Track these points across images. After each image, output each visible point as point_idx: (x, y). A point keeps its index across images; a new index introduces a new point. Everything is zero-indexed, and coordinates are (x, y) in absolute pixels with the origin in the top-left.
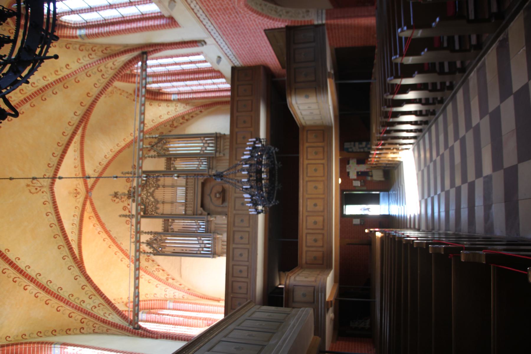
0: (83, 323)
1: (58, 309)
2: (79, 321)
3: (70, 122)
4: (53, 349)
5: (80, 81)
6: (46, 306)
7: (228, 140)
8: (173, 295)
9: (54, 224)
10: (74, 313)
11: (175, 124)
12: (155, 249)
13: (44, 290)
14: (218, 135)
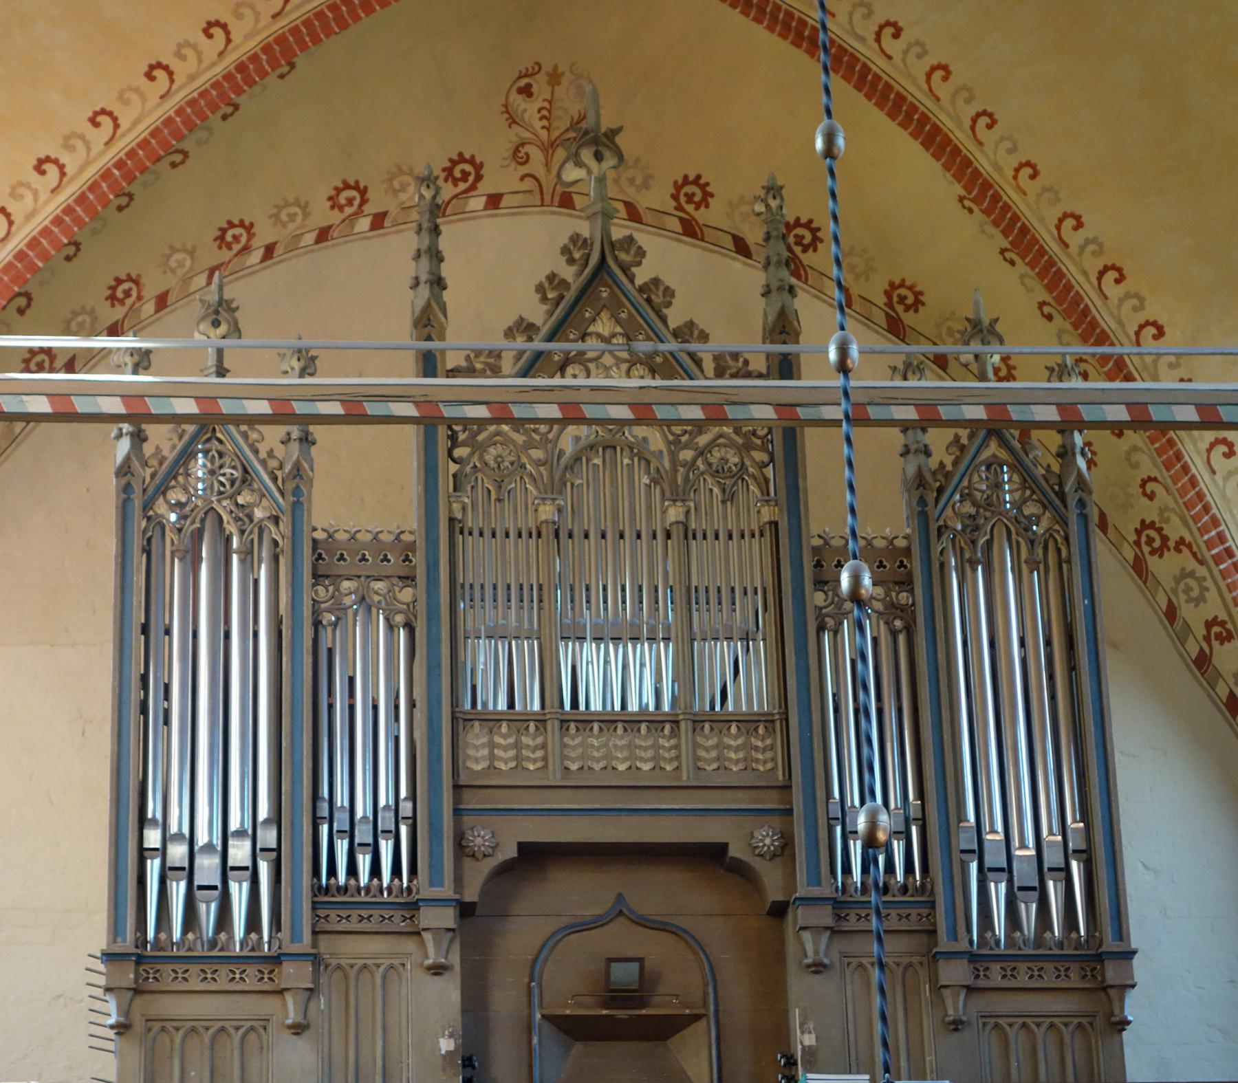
11: (1164, 567)
12: (172, 474)
14: (1112, 973)
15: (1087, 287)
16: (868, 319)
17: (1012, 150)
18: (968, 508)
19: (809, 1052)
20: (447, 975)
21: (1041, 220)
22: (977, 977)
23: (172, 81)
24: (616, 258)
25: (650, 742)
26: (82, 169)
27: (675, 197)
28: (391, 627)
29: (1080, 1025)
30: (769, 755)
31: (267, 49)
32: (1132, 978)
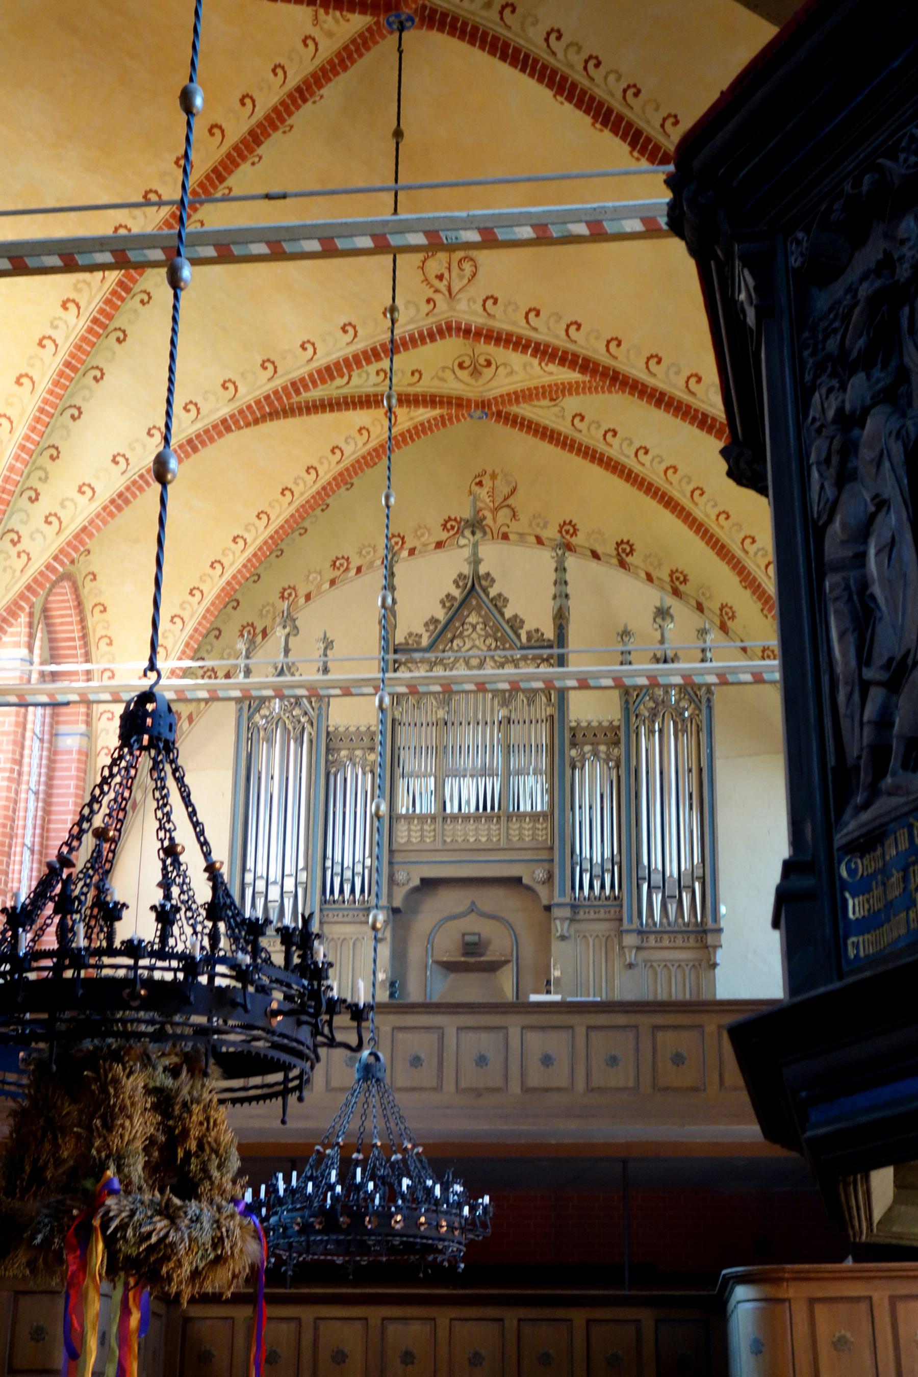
3: (699, 380)
7: (678, 991)
9: (315, 353)
14: (710, 939)
15: (760, 573)
17: (714, 506)
18: (652, 704)
19: (558, 980)
20: (384, 942)
21: (733, 540)
22: (642, 942)
23: (293, 496)
24: (481, 586)
25: (486, 827)
26: (255, 540)
27: (560, 532)
28: (364, 773)
29: (694, 966)
30: (544, 832)
31: (335, 479)
32: (720, 941)
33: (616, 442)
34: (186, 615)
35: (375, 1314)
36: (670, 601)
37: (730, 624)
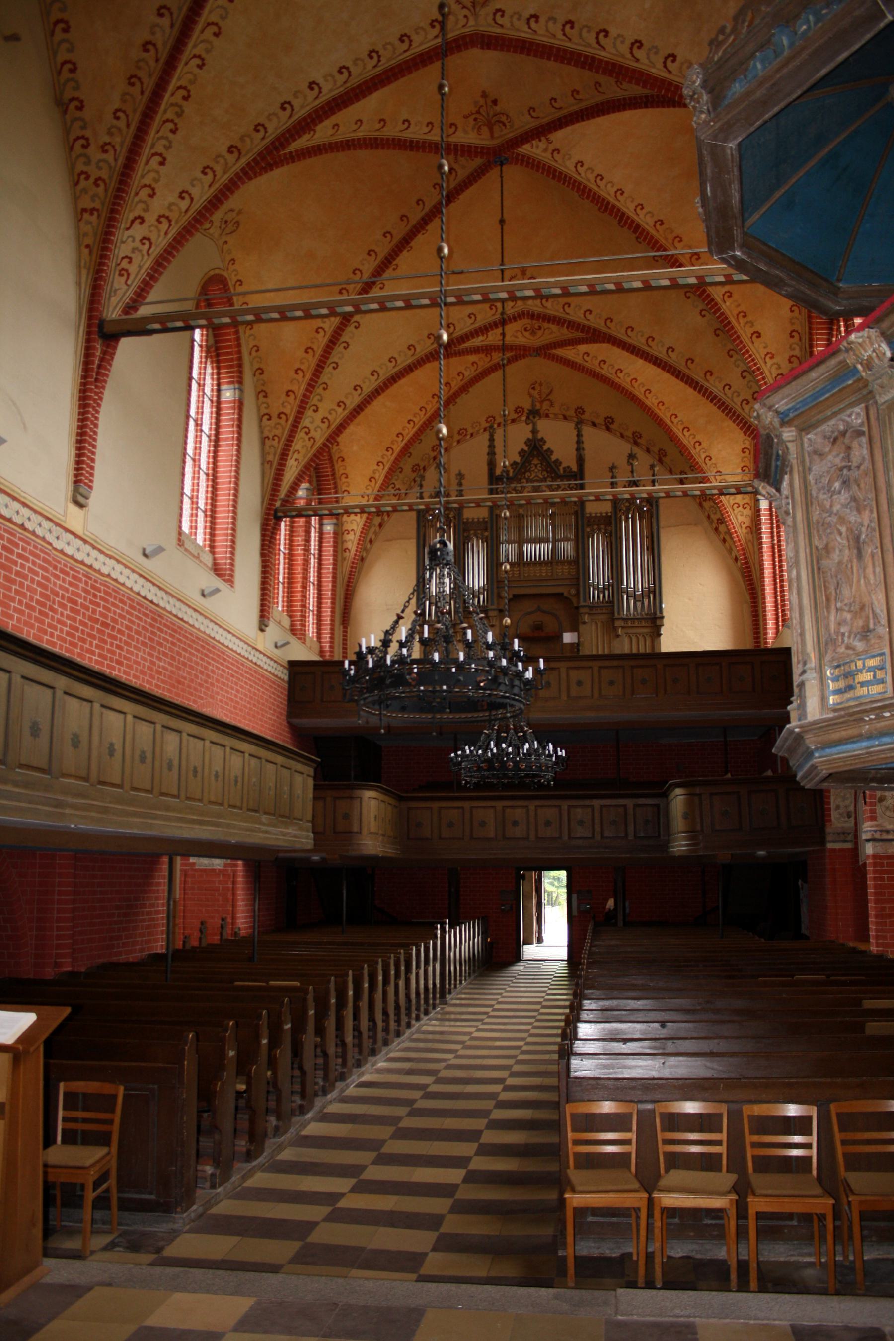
0: (279, 417)
1: (299, 371)
2: (282, 410)
4: (232, 386)
5: (733, 359)
6: (303, 349)
7: (643, 647)
8: (350, 529)
10: (295, 399)
11: (706, 504)
13: (330, 341)
16: (628, 441)
33: (605, 367)
34: (385, 461)
35: (499, 804)
36: (636, 450)
37: (663, 459)
